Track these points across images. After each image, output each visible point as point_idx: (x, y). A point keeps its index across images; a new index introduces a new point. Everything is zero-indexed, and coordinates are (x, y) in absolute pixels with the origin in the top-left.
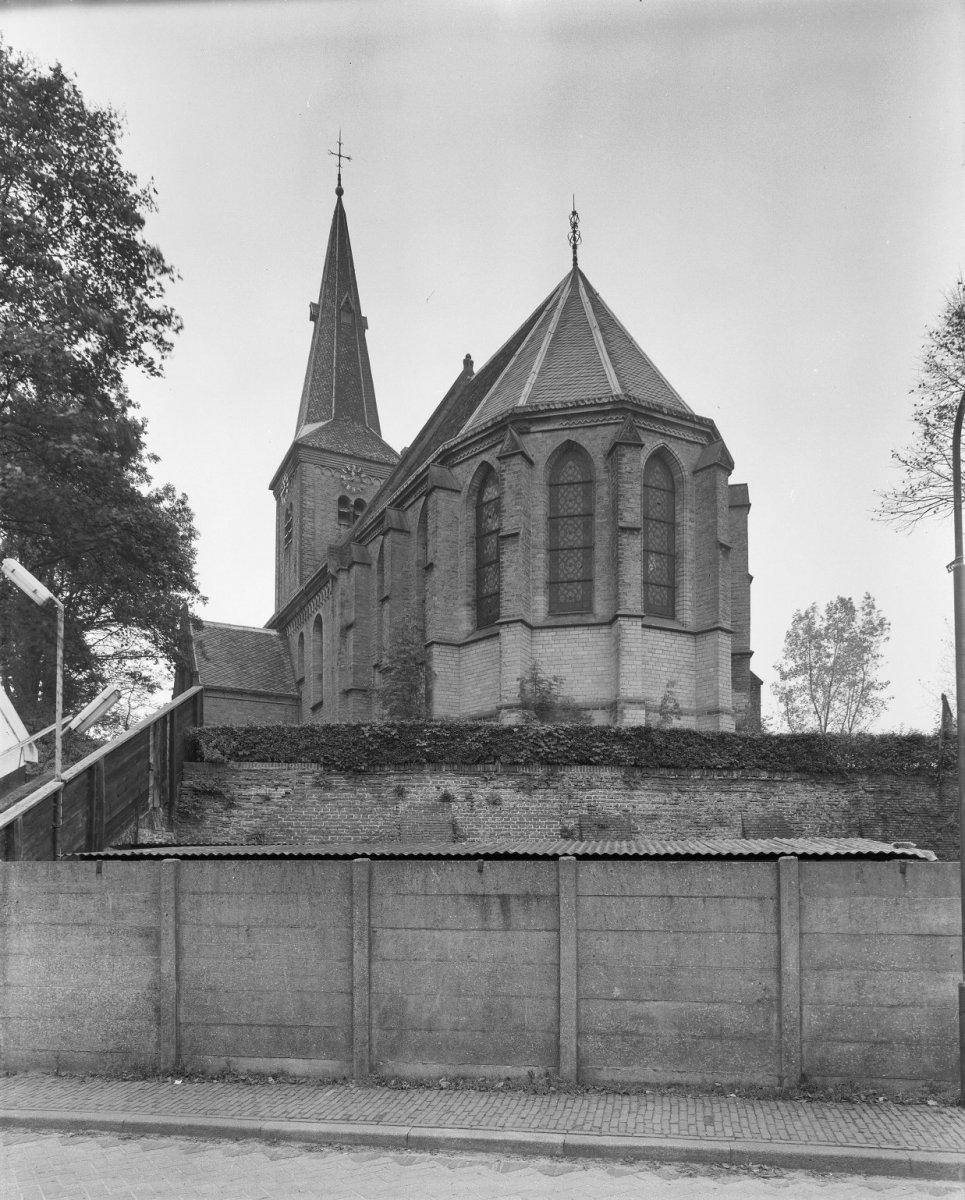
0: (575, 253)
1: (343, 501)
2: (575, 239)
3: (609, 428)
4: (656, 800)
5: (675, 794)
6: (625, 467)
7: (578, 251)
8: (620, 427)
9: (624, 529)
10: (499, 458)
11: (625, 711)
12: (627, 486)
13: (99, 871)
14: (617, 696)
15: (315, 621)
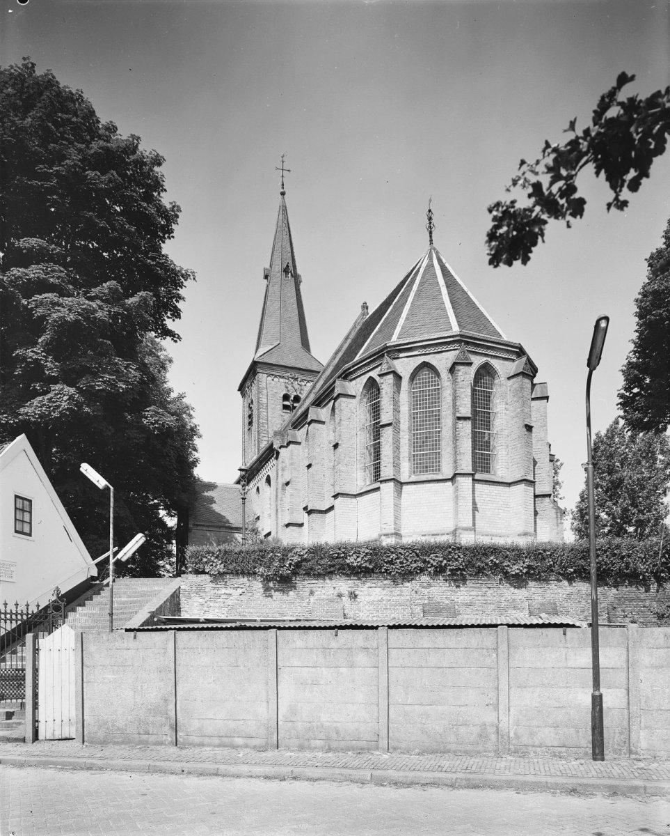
0: (431, 236)
1: (286, 397)
2: (430, 227)
3: (451, 352)
4: (472, 593)
5: (485, 590)
6: (460, 379)
7: (433, 235)
8: (457, 352)
9: (459, 418)
10: (380, 375)
11: (461, 536)
12: (462, 390)
13: (135, 637)
14: (457, 526)
15: (266, 479)
